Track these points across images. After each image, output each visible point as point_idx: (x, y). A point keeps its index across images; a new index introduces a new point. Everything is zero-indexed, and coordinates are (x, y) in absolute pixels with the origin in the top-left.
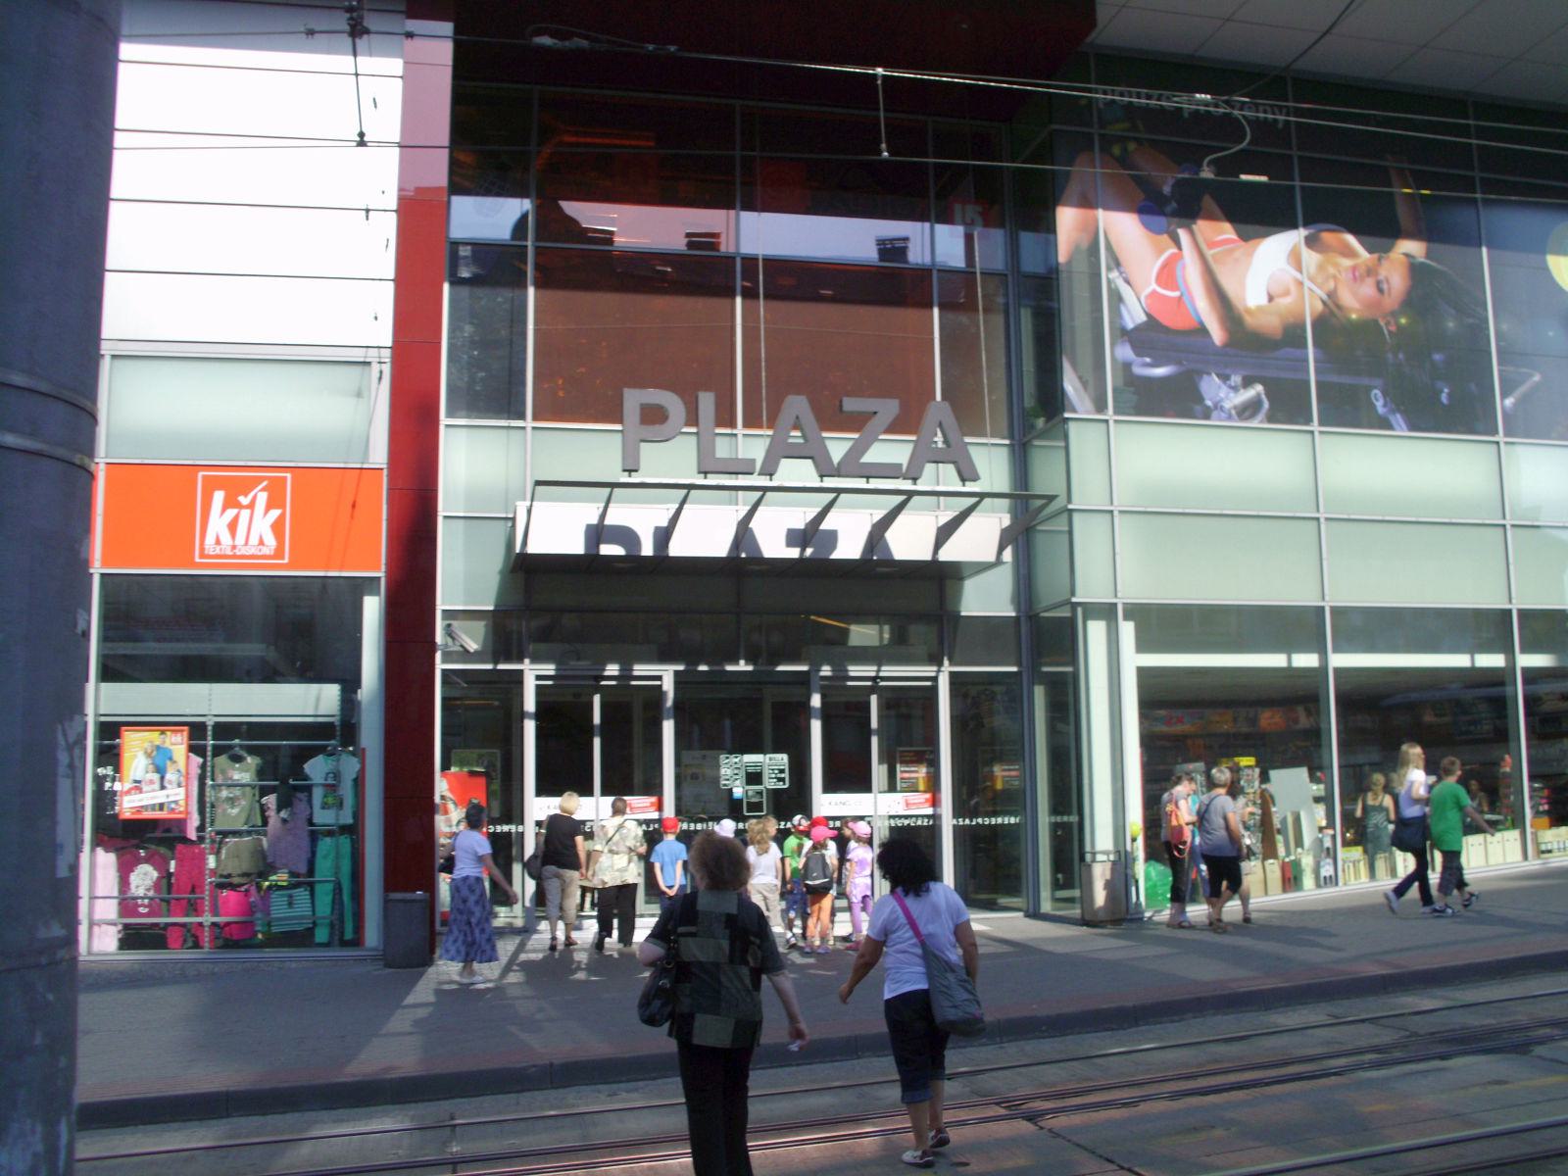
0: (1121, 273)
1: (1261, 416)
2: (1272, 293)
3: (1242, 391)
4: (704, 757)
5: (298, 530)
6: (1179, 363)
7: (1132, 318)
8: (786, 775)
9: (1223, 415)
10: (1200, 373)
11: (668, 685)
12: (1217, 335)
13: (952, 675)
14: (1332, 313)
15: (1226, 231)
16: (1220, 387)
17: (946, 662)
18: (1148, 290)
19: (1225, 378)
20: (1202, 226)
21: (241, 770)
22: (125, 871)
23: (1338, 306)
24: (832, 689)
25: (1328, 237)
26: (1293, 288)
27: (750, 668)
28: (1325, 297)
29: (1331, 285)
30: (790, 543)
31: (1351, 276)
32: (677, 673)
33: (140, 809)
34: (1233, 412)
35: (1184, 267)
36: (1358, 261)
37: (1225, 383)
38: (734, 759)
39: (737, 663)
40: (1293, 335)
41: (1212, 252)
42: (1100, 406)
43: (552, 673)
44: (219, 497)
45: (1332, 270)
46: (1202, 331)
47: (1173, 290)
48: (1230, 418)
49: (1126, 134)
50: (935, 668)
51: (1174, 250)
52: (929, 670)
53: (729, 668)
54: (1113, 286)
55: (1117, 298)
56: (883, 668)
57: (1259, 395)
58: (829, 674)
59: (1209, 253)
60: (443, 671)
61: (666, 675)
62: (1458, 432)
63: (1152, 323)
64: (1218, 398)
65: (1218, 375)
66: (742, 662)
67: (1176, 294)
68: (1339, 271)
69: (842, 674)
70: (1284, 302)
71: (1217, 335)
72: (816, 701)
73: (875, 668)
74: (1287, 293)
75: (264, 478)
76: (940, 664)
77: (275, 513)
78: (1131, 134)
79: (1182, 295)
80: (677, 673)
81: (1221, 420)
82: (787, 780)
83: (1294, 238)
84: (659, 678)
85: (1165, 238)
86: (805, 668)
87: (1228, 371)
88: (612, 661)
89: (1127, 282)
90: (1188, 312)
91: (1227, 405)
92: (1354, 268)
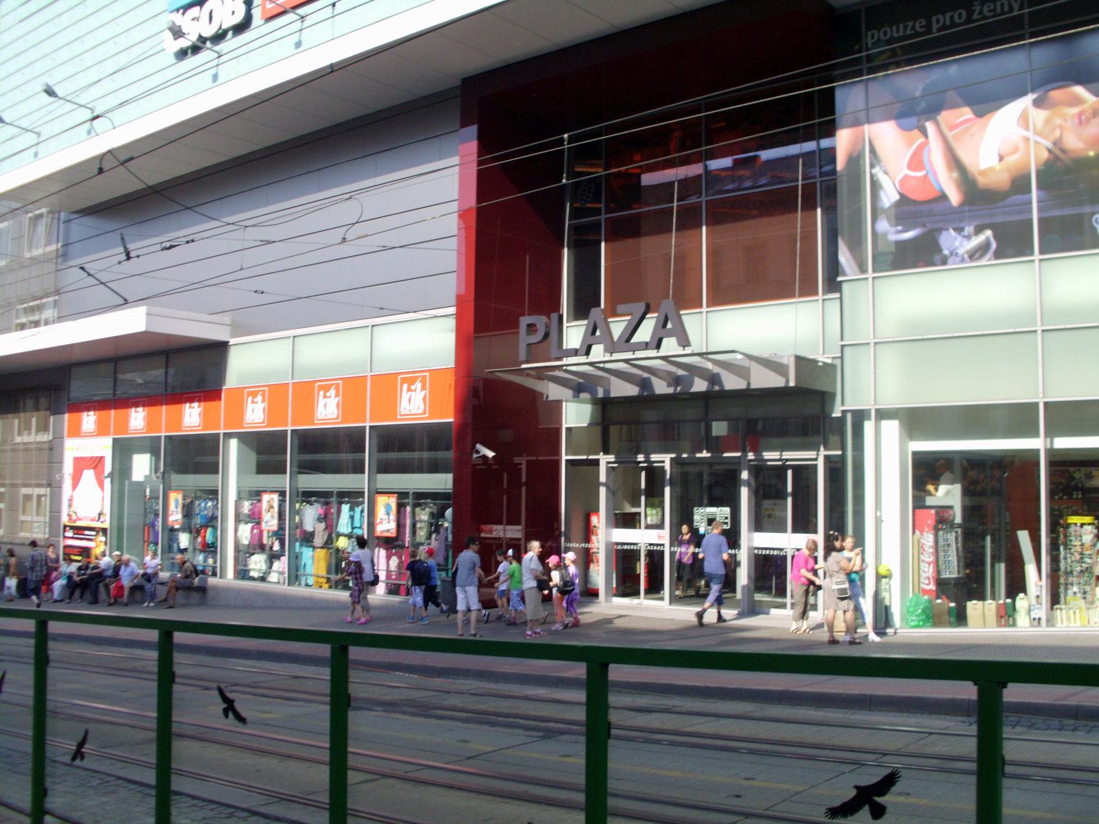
0: (881, 168)
1: (990, 254)
2: (1002, 153)
3: (974, 238)
4: (775, 504)
5: (273, 411)
6: (924, 225)
7: (889, 199)
8: (728, 521)
9: (957, 259)
10: (940, 230)
11: (667, 466)
12: (955, 197)
13: (826, 457)
14: (1057, 158)
15: (966, 113)
16: (955, 239)
17: (822, 448)
18: (902, 175)
19: (959, 230)
20: (946, 116)
21: (424, 515)
22: (388, 558)
23: (1063, 151)
24: (759, 470)
25: (1056, 94)
26: (1022, 146)
27: (709, 455)
28: (1050, 145)
29: (1057, 133)
30: (669, 385)
31: (1076, 121)
32: (671, 459)
33: (383, 531)
34: (966, 256)
35: (929, 151)
36: (1085, 106)
37: (959, 234)
38: (701, 510)
39: (701, 452)
40: (1020, 184)
41: (953, 133)
42: (863, 269)
43: (613, 460)
44: (405, 386)
45: (1058, 121)
46: (943, 197)
47: (920, 170)
48: (963, 261)
49: (887, 62)
50: (815, 453)
51: (922, 140)
52: (811, 454)
53: (698, 455)
54: (875, 178)
55: (875, 185)
56: (784, 453)
57: (988, 239)
58: (753, 458)
59: (950, 135)
60: (567, 460)
61: (664, 460)
62: (916, 267)
63: (904, 200)
64: (954, 247)
65: (955, 229)
66: (705, 452)
67: (922, 173)
68: (1066, 120)
69: (759, 457)
70: (1013, 160)
71: (955, 197)
72: (745, 475)
73: (779, 453)
74: (1016, 150)
75: (333, 384)
76: (818, 450)
77: (424, 392)
78: (892, 60)
79: (927, 173)
80: (671, 459)
81: (955, 264)
82: (729, 524)
83: (1027, 101)
84: (663, 462)
85: (916, 132)
86: (738, 454)
87: (962, 225)
88: (685, 453)
89: (886, 173)
90: (931, 185)
91: (961, 251)
92: (1080, 115)
